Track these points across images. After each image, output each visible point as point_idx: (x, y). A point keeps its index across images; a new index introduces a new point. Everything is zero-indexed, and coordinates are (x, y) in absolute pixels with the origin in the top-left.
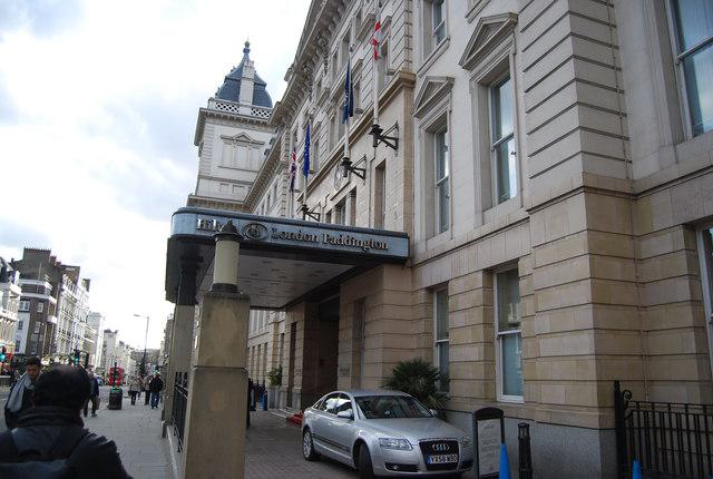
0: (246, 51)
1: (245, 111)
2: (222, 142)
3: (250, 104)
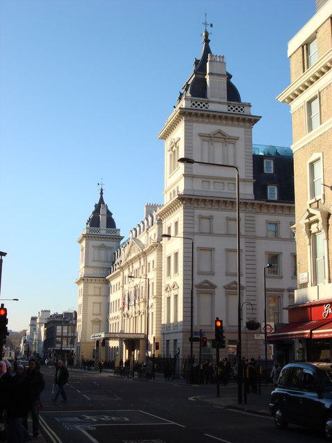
0: (102, 193)
2: (199, 138)
3: (226, 101)
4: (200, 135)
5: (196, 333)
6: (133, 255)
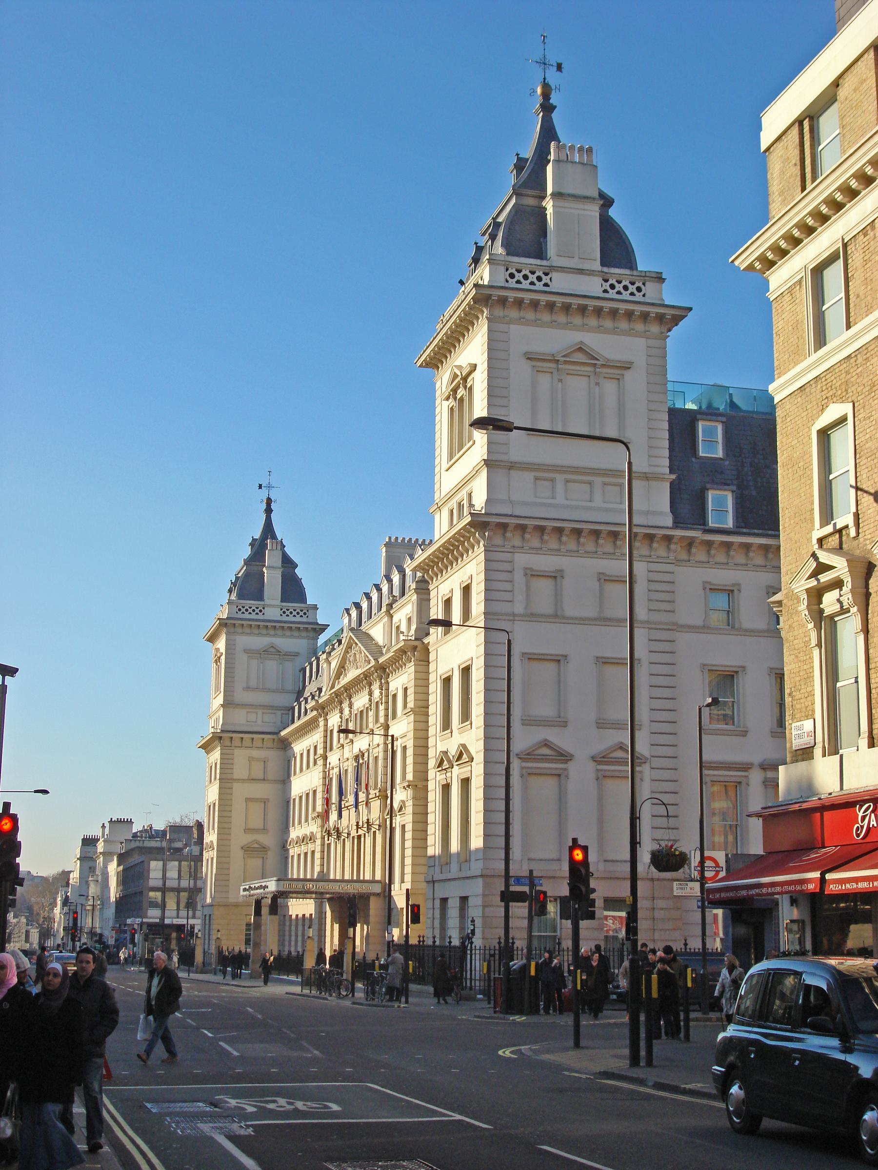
0: (269, 511)
1: (273, 613)
3: (597, 266)
4: (530, 357)
5: (518, 881)
6: (352, 674)
